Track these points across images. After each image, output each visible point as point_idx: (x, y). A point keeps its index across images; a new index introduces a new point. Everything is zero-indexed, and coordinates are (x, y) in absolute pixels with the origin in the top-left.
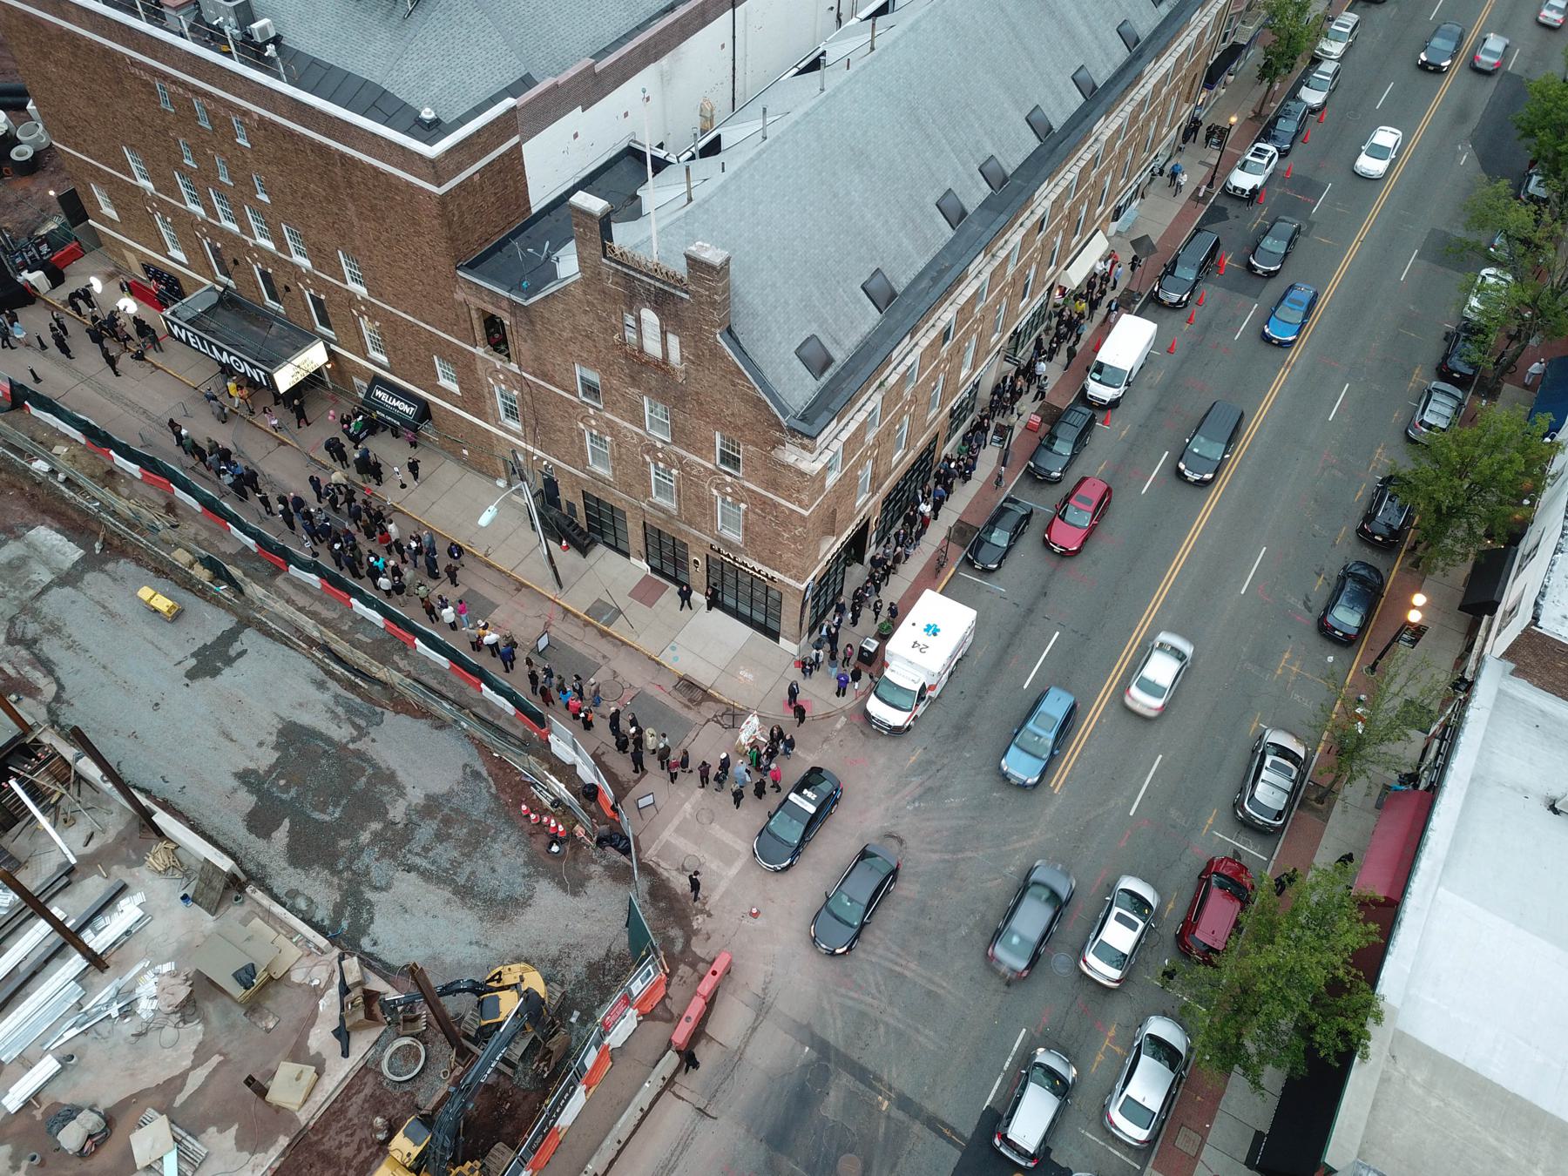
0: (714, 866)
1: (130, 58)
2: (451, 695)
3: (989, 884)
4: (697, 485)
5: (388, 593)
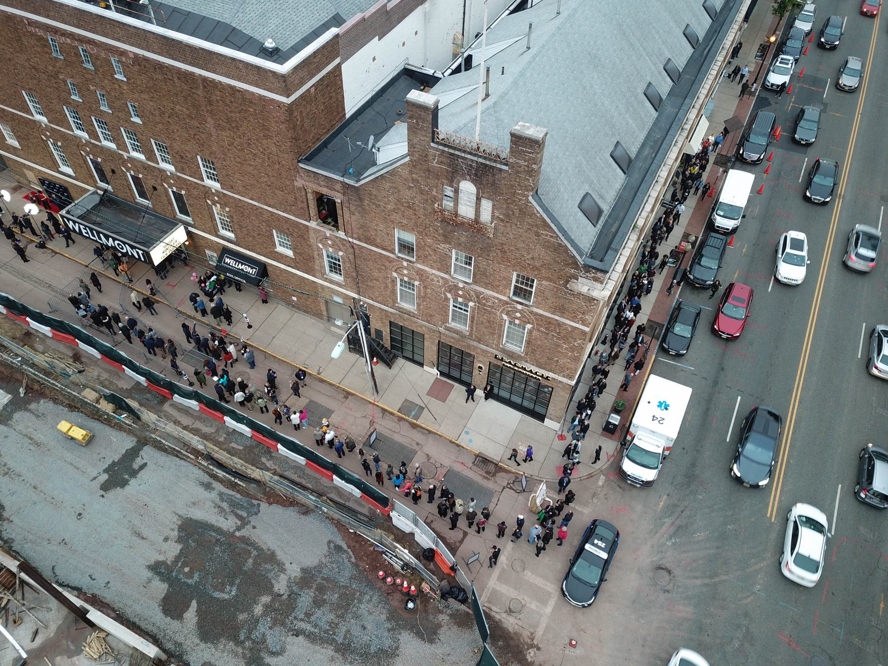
0: (533, 606)
1: (28, 19)
2: (309, 486)
3: (745, 601)
4: (490, 313)
5: (242, 403)
